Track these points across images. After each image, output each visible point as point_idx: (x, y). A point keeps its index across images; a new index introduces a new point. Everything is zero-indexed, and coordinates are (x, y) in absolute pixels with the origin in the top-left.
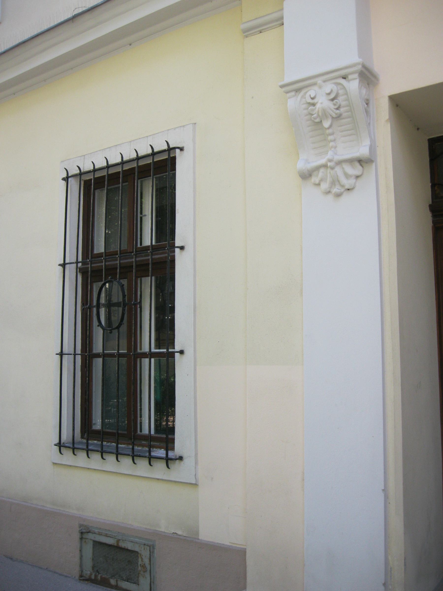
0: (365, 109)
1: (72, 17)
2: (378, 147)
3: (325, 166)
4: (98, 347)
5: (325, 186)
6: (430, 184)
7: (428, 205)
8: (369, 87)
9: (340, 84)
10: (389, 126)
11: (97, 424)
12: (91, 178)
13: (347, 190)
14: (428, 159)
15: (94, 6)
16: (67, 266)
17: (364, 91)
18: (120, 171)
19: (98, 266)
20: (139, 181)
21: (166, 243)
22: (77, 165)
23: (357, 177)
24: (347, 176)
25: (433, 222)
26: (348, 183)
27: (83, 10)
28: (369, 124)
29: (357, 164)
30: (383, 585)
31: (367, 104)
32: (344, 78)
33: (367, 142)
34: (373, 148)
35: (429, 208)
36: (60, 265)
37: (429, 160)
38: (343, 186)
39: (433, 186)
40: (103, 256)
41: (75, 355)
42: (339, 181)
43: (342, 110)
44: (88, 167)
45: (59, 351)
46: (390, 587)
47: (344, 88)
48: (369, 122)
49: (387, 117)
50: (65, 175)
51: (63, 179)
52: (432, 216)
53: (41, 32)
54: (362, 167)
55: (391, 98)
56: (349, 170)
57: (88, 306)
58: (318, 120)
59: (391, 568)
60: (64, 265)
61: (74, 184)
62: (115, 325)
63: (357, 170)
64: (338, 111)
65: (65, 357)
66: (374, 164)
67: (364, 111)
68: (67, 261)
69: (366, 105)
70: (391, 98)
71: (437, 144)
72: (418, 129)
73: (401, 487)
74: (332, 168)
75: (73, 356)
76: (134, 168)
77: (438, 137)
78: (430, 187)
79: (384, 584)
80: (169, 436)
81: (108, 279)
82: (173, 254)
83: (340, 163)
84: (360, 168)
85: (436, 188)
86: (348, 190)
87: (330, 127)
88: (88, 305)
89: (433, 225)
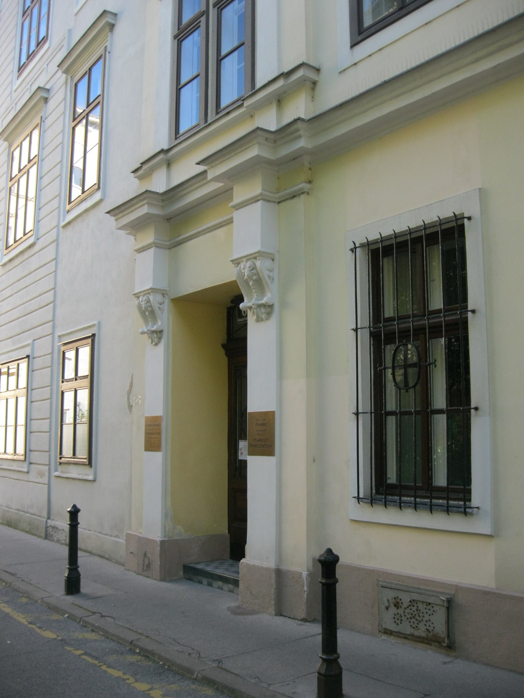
1: (384, 82)
4: (391, 405)
11: (392, 477)
12: (437, 230)
15: (488, 30)
16: (359, 331)
18: (438, 231)
19: (452, 320)
20: (427, 248)
21: (458, 306)
22: (353, 241)
27: (437, 54)
36: (353, 329)
40: (442, 312)
41: (371, 413)
44: (373, 236)
45: (355, 411)
50: (353, 246)
51: (352, 250)
53: (369, 89)
57: (428, 363)
60: (356, 330)
61: (361, 253)
62: (411, 384)
65: (361, 417)
68: (359, 327)
75: (370, 414)
76: (454, 227)
80: (389, 482)
81: (403, 342)
82: (466, 316)
88: (383, 366)
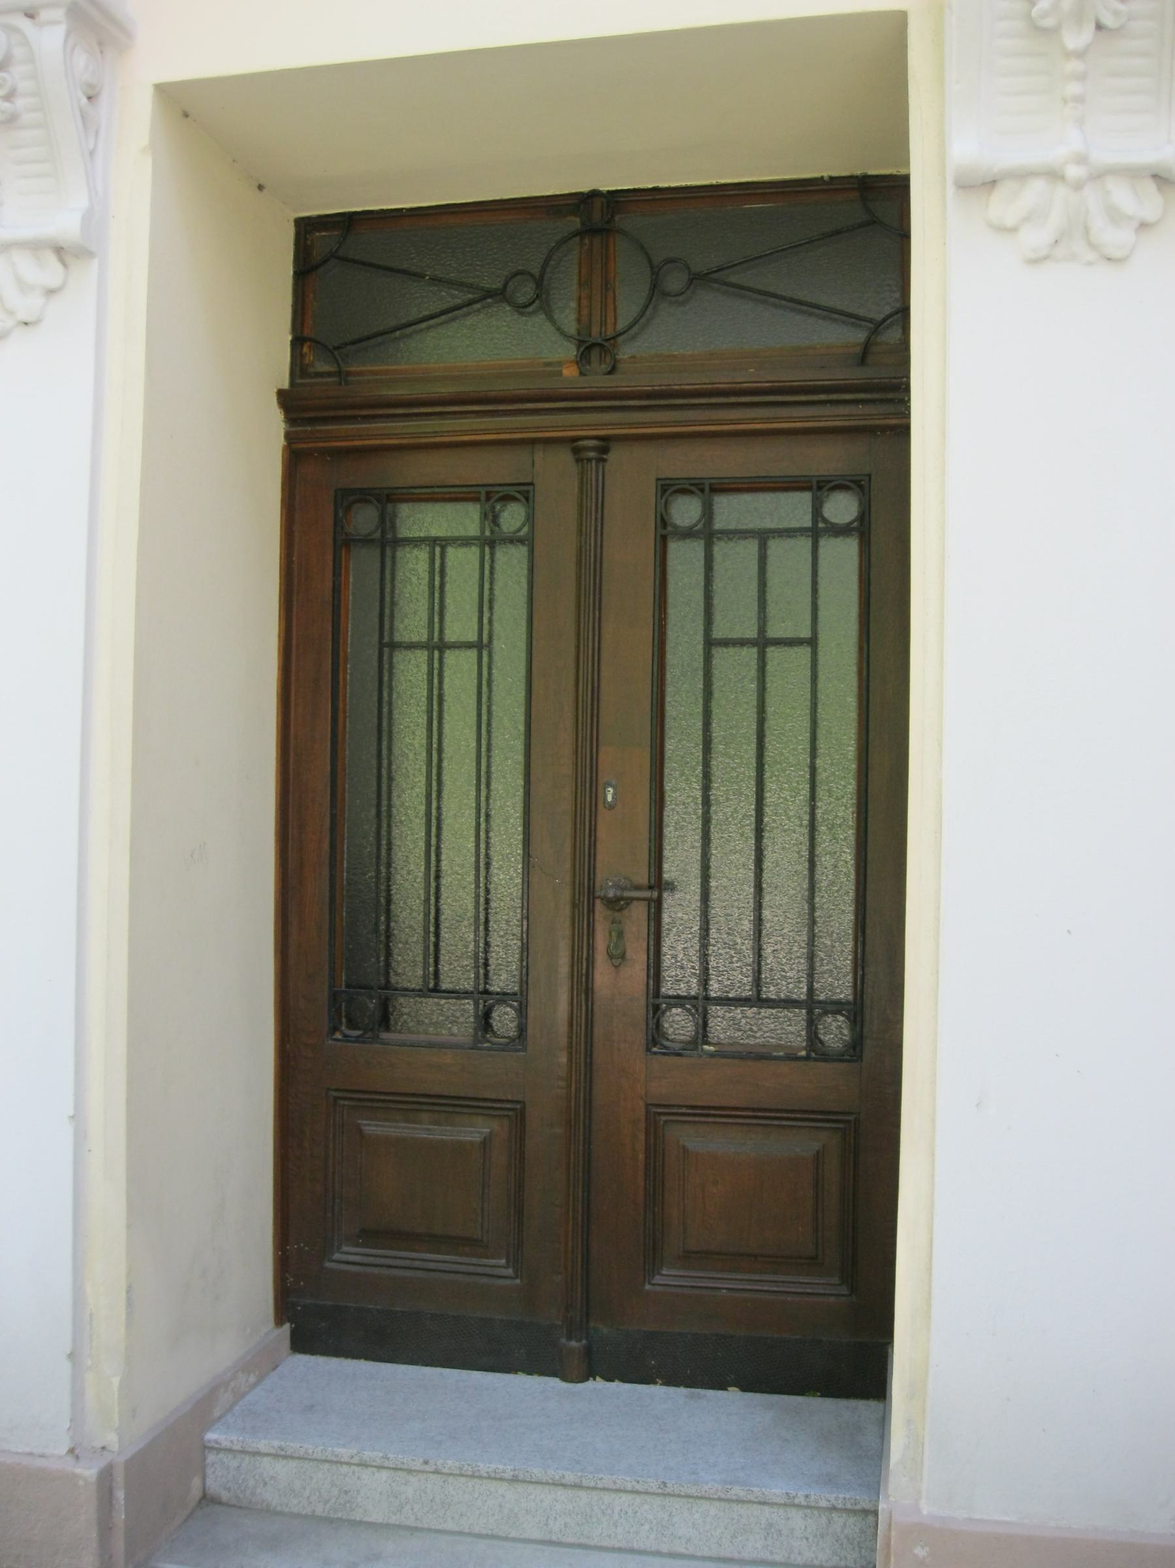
0: (81, 110)
2: (113, 217)
3: (1054, 175)
5: (1036, 238)
6: (290, 338)
7: (276, 390)
8: (102, 52)
9: (17, 30)
10: (147, 163)
13: (24, 325)
14: (290, 272)
17: (81, 60)
23: (50, 292)
24: (24, 287)
25: (288, 436)
26: (26, 306)
28: (92, 153)
29: (51, 259)
30: (69, 1358)
31: (89, 98)
32: (30, 15)
33: (81, 201)
34: (93, 219)
35: (278, 399)
37: (292, 273)
38: (11, 313)
39: (298, 342)
42: (1087, 230)
43: (20, 103)
46: (89, 1362)
47: (26, 43)
48: (91, 146)
49: (145, 141)
52: (285, 422)
54: (65, 265)
55: (165, 93)
56: (1123, 196)
58: (1049, 22)
59: (91, 1315)
63: (50, 272)
64: (7, 105)
66: (95, 263)
67: (78, 113)
69: (84, 100)
70: (165, 93)
71: (317, 234)
72: (260, 187)
73: (121, 1109)
74: (1078, 186)
77: (320, 217)
78: (289, 343)
79: (71, 1356)
83: (1100, 175)
84: (59, 267)
85: (305, 349)
86: (26, 324)
87: (1080, 55)
89: (285, 443)
